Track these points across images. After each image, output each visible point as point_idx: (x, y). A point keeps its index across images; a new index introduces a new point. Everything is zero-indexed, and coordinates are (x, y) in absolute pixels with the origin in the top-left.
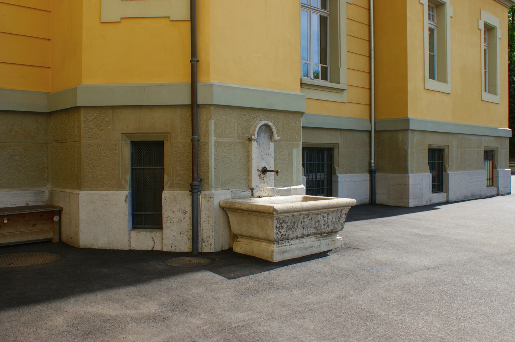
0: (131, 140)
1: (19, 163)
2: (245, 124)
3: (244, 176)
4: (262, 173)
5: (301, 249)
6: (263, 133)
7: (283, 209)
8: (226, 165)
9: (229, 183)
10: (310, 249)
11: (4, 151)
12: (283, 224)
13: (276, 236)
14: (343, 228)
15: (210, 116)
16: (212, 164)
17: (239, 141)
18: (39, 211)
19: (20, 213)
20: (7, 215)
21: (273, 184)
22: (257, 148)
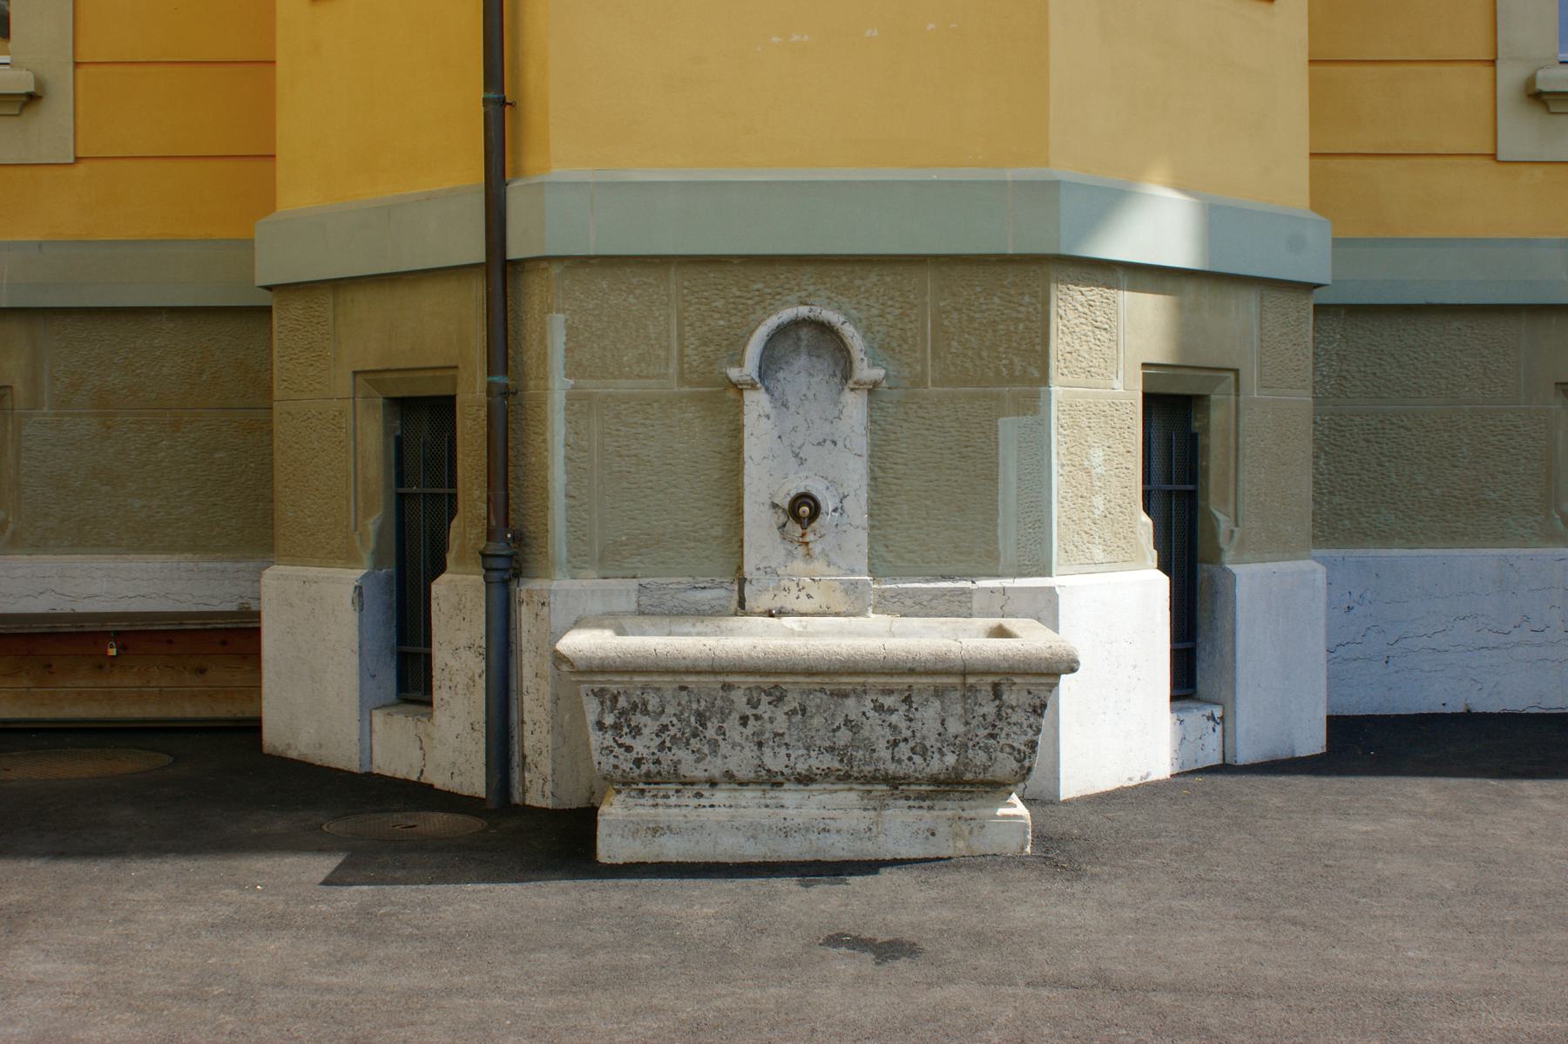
0: (385, 396)
1: (227, 473)
2: (721, 323)
3: (719, 528)
4: (791, 519)
5: (754, 831)
6: (804, 357)
7: (600, 654)
8: (625, 485)
9: (640, 555)
10: (813, 837)
11: (179, 434)
12: (633, 718)
13: (603, 759)
14: (1030, 769)
15: (549, 300)
16: (558, 477)
17: (686, 389)
18: (209, 627)
19: (150, 628)
20: (118, 633)
21: (863, 564)
22: (768, 417)
